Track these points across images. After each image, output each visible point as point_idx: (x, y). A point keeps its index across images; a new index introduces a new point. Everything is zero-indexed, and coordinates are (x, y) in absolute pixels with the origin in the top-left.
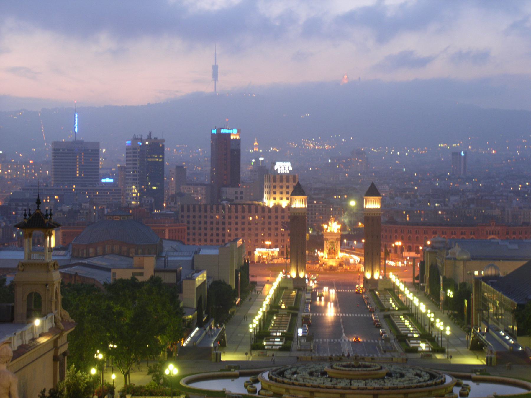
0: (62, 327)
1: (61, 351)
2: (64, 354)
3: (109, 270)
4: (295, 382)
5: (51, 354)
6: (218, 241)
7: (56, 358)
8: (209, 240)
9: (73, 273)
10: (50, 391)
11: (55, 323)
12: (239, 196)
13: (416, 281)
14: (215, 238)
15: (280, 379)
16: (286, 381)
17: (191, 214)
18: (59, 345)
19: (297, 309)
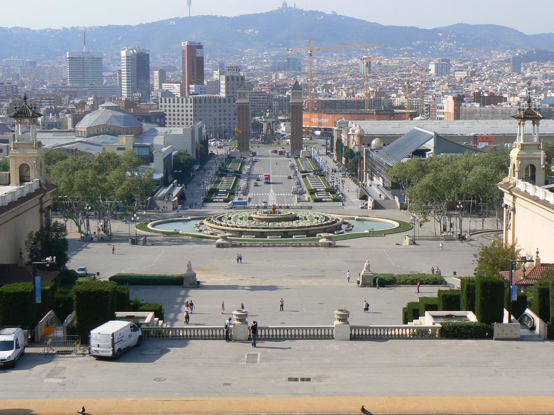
0: (45, 188)
1: (46, 205)
2: (49, 207)
3: (101, 146)
4: (229, 225)
5: (38, 207)
6: (183, 124)
7: (42, 211)
8: (185, 123)
9: (74, 149)
10: (36, 234)
11: (40, 185)
12: (203, 90)
13: (328, 151)
14: (176, 121)
15: (219, 222)
16: (222, 223)
17: (180, 104)
18: (43, 201)
19: (241, 173)
